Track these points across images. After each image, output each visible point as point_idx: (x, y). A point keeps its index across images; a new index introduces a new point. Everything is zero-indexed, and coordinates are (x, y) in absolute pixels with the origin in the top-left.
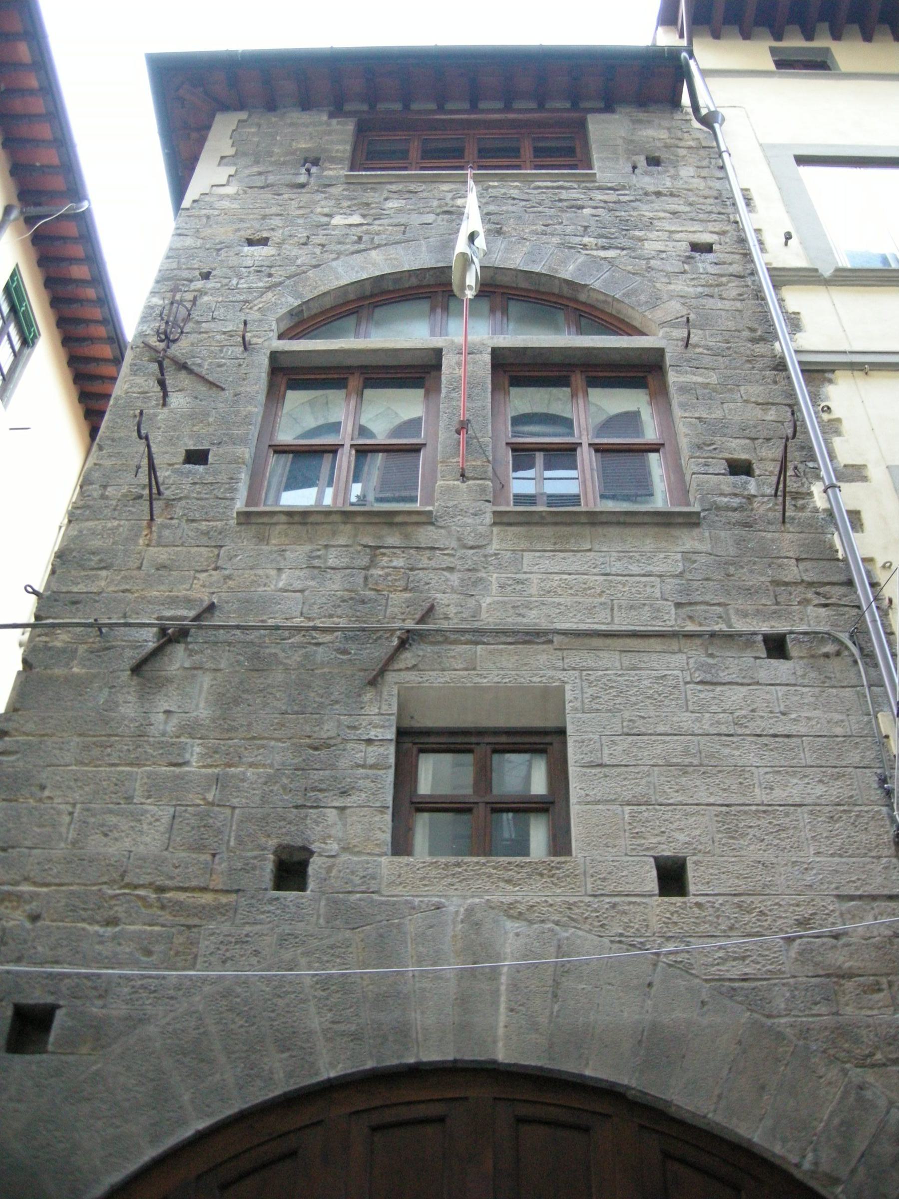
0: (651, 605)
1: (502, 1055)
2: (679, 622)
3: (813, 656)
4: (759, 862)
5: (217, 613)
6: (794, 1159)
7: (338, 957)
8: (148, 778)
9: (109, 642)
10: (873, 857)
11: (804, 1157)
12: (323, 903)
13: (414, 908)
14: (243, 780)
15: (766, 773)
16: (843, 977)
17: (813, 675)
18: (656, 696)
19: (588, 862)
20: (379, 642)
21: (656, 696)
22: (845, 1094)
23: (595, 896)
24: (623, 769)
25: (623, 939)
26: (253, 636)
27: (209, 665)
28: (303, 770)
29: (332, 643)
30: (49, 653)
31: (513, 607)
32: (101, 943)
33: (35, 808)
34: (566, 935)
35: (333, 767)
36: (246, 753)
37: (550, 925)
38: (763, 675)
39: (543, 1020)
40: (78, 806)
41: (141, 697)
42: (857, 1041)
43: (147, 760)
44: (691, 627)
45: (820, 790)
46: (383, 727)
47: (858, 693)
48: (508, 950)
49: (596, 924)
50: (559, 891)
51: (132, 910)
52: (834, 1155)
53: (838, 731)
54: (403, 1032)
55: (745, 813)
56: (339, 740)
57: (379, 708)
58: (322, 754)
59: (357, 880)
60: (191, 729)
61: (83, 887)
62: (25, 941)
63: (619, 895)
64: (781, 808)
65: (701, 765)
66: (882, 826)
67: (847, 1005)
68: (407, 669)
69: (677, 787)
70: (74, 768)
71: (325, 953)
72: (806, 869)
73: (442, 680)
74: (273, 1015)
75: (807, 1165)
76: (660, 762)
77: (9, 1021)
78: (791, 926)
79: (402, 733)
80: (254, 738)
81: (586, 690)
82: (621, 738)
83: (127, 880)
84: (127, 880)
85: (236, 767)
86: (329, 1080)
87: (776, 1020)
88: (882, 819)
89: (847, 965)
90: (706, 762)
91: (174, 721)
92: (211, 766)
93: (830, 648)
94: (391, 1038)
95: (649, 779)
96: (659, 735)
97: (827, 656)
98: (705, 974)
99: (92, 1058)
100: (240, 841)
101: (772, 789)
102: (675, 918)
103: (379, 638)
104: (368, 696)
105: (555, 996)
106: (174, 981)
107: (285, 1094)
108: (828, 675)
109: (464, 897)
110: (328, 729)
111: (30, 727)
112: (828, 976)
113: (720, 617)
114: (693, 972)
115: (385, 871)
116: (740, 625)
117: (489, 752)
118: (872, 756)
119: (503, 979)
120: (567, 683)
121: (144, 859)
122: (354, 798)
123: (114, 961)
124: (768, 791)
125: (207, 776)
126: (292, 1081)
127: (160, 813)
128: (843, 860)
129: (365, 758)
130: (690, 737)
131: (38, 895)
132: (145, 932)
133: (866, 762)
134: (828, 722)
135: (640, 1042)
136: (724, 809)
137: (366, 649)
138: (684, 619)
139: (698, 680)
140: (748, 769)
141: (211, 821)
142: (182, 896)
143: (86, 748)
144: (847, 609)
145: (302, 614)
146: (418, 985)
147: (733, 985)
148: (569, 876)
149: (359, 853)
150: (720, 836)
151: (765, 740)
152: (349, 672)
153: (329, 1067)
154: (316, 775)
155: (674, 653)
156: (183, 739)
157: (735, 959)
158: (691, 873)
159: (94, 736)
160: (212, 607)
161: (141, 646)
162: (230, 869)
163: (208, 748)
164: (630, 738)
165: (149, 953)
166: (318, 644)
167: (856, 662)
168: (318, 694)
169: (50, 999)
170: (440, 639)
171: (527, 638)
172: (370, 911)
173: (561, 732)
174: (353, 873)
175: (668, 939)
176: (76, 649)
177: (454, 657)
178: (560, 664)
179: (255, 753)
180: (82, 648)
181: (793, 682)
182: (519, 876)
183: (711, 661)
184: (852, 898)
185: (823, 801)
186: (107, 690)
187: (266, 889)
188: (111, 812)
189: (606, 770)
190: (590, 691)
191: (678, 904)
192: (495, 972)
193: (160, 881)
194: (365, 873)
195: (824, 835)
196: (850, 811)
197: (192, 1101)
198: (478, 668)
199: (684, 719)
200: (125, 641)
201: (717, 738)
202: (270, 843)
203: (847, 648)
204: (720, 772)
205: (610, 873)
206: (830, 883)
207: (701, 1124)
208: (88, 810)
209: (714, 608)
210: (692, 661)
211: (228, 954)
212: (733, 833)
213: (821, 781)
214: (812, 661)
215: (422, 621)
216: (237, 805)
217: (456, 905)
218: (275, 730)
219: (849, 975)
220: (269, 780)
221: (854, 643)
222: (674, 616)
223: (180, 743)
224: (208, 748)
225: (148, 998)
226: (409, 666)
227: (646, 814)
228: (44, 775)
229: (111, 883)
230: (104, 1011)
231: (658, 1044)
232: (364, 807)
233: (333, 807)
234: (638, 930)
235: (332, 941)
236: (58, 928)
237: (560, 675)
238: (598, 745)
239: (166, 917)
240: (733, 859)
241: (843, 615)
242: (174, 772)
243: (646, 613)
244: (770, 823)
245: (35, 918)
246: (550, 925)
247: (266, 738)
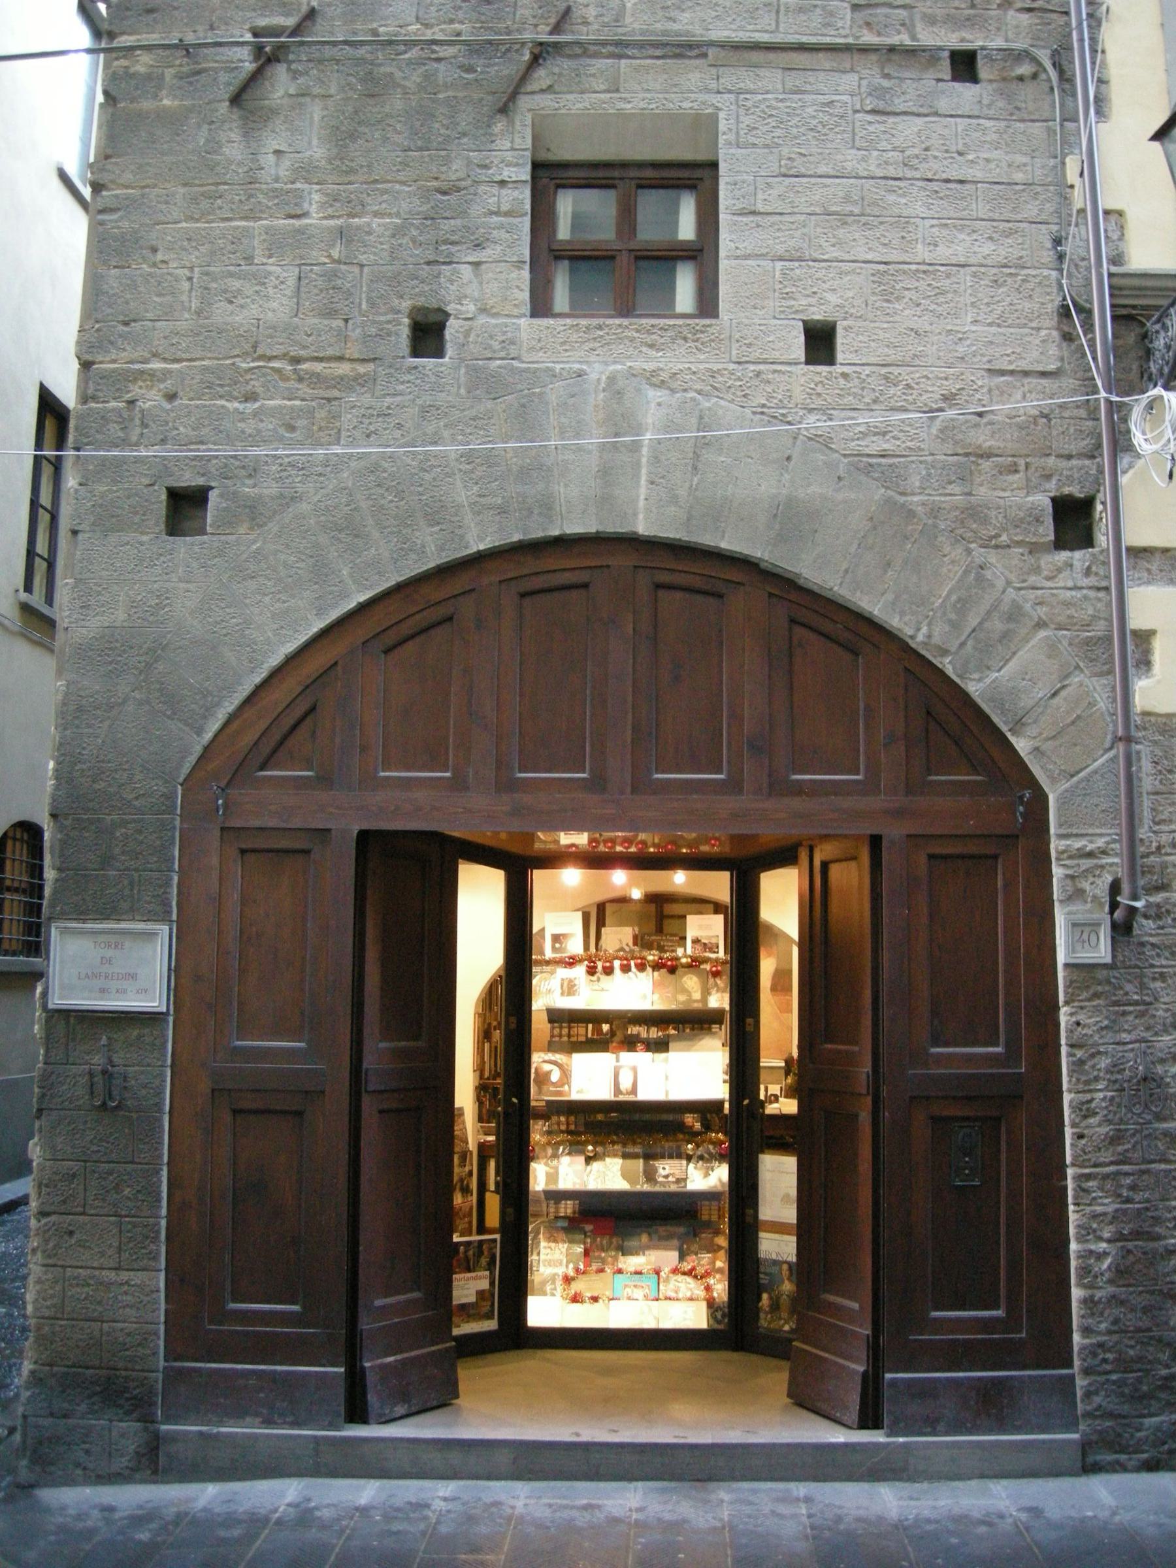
0: (824, 8)
1: (643, 528)
2: (854, 30)
3: (1004, 79)
4: (912, 329)
5: (319, 20)
6: (909, 631)
7: (481, 429)
8: (267, 233)
9: (197, 63)
10: (1032, 328)
11: (919, 630)
12: (463, 371)
13: (555, 376)
14: (369, 233)
15: (933, 226)
16: (981, 456)
17: (1001, 104)
18: (820, 128)
19: (734, 325)
20: (509, 55)
21: (820, 128)
22: (966, 572)
23: (739, 363)
24: (778, 218)
25: (765, 410)
26: (362, 51)
27: (316, 90)
28: (433, 219)
29: (455, 57)
30: (133, 82)
31: (663, 8)
32: (243, 420)
33: (150, 274)
34: (707, 404)
35: (464, 214)
36: (369, 200)
37: (692, 394)
38: (943, 105)
39: (682, 492)
40: (196, 270)
41: (246, 135)
42: (985, 521)
43: (261, 211)
44: (869, 38)
45: (987, 248)
46: (517, 165)
47: (1049, 128)
48: (650, 421)
49: (739, 393)
50: (702, 357)
51: (269, 385)
52: (947, 629)
53: (1019, 177)
54: (547, 506)
55: (904, 272)
56: (469, 182)
57: (512, 142)
58: (452, 198)
59: (496, 345)
60: (306, 172)
61: (216, 362)
62: (167, 423)
63: (765, 362)
64: (942, 269)
65: (863, 215)
66: (1048, 294)
67: (981, 485)
68: (542, 91)
69: (834, 240)
70: (184, 225)
71: (467, 425)
72: (960, 339)
73: (580, 106)
74: (421, 489)
75: (920, 637)
76: (818, 210)
77: (165, 503)
78: (936, 402)
79: (538, 167)
80: (376, 181)
81: (742, 119)
82: (777, 179)
83: (259, 352)
84: (259, 352)
85: (360, 217)
86: (479, 551)
87: (909, 498)
88: (1049, 286)
89: (988, 444)
90: (868, 211)
91: (286, 163)
92: (332, 217)
93: (1025, 69)
94: (536, 512)
95: (805, 230)
96: (820, 177)
97: (1021, 79)
98: (844, 449)
99: (251, 537)
100: (372, 304)
101: (936, 245)
102: (819, 389)
103: (508, 50)
104: (499, 126)
105: (695, 468)
106: (321, 458)
107: (438, 566)
108: (1019, 104)
109: (606, 364)
110: (456, 170)
111: (128, 177)
112: (967, 455)
113: (903, 25)
114: (833, 446)
115: (524, 336)
116: (928, 37)
117: (634, 187)
118: (1051, 210)
119: (645, 451)
120: (721, 109)
121: (274, 328)
122: (489, 251)
123: (257, 439)
124: (932, 247)
125: (329, 229)
126: (444, 554)
127: (286, 275)
128: (1000, 330)
129: (499, 203)
130: (852, 181)
131: (170, 372)
132: (285, 406)
133: (1043, 217)
134: (1009, 166)
135: (775, 515)
136: (881, 267)
137: (495, 64)
138: (860, 27)
139: (869, 108)
140: (912, 220)
141: (339, 282)
142: (318, 367)
143: (194, 200)
144: (1054, 16)
145: (417, 18)
146: (561, 457)
147: (870, 460)
148: (713, 341)
149: (496, 315)
150: (875, 298)
151: (935, 186)
152: (475, 96)
153: (479, 539)
154: (447, 225)
155: (844, 72)
156: (298, 185)
157: (875, 434)
158: (841, 340)
159: (202, 185)
160: (312, 14)
161: (236, 68)
162: (365, 336)
163: (327, 195)
164: (788, 180)
165: (292, 429)
166: (438, 60)
167: (1052, 89)
168: (443, 125)
169: (201, 481)
170: (578, 51)
171: (678, 51)
172: (511, 380)
173: (714, 165)
174: (491, 337)
175: (811, 410)
176: (163, 74)
177: (593, 75)
178: (713, 85)
179: (380, 200)
180: (169, 73)
181: (976, 113)
182: (662, 341)
183: (886, 83)
184: (1002, 373)
185: (989, 262)
186: (206, 126)
187: (403, 357)
188: (231, 275)
189: (759, 218)
190: (746, 121)
191: (824, 374)
192: (635, 447)
193: (295, 351)
194: (504, 338)
195: (986, 301)
196: (1016, 275)
197: (351, 575)
198: (622, 90)
199: (849, 158)
200: (216, 61)
201: (883, 182)
202: (404, 304)
203: (1045, 70)
204: (881, 223)
205: (756, 338)
206: (982, 355)
207: (829, 595)
208: (207, 274)
209: (897, 11)
210: (864, 83)
211: (372, 428)
212: (889, 296)
213: (991, 238)
214: (1002, 85)
215: (557, 29)
216: (365, 262)
217: (597, 372)
218: (399, 170)
219: (987, 455)
220: (398, 232)
221: (1054, 65)
222: (849, 23)
223: (296, 190)
224: (327, 195)
225: (298, 476)
226: (544, 87)
227: (798, 272)
228: (154, 235)
229: (245, 354)
230: (256, 490)
231: (791, 518)
232: (500, 261)
233: (469, 263)
234: (780, 401)
235: (473, 412)
236: (197, 407)
237: (714, 99)
238: (752, 188)
239: (304, 389)
240: (885, 325)
241: (1049, 24)
242: (293, 225)
243: (817, 18)
244: (929, 285)
245: (171, 397)
246: (692, 394)
247: (389, 181)
